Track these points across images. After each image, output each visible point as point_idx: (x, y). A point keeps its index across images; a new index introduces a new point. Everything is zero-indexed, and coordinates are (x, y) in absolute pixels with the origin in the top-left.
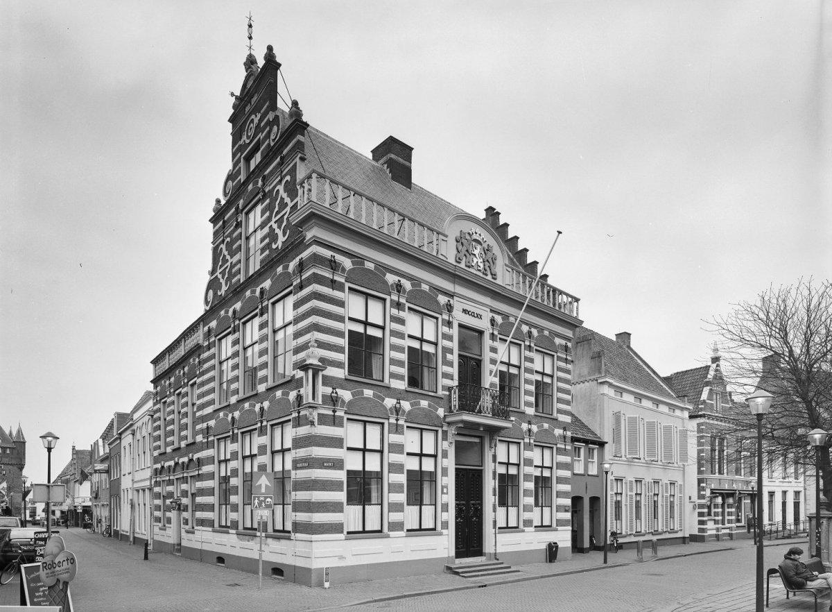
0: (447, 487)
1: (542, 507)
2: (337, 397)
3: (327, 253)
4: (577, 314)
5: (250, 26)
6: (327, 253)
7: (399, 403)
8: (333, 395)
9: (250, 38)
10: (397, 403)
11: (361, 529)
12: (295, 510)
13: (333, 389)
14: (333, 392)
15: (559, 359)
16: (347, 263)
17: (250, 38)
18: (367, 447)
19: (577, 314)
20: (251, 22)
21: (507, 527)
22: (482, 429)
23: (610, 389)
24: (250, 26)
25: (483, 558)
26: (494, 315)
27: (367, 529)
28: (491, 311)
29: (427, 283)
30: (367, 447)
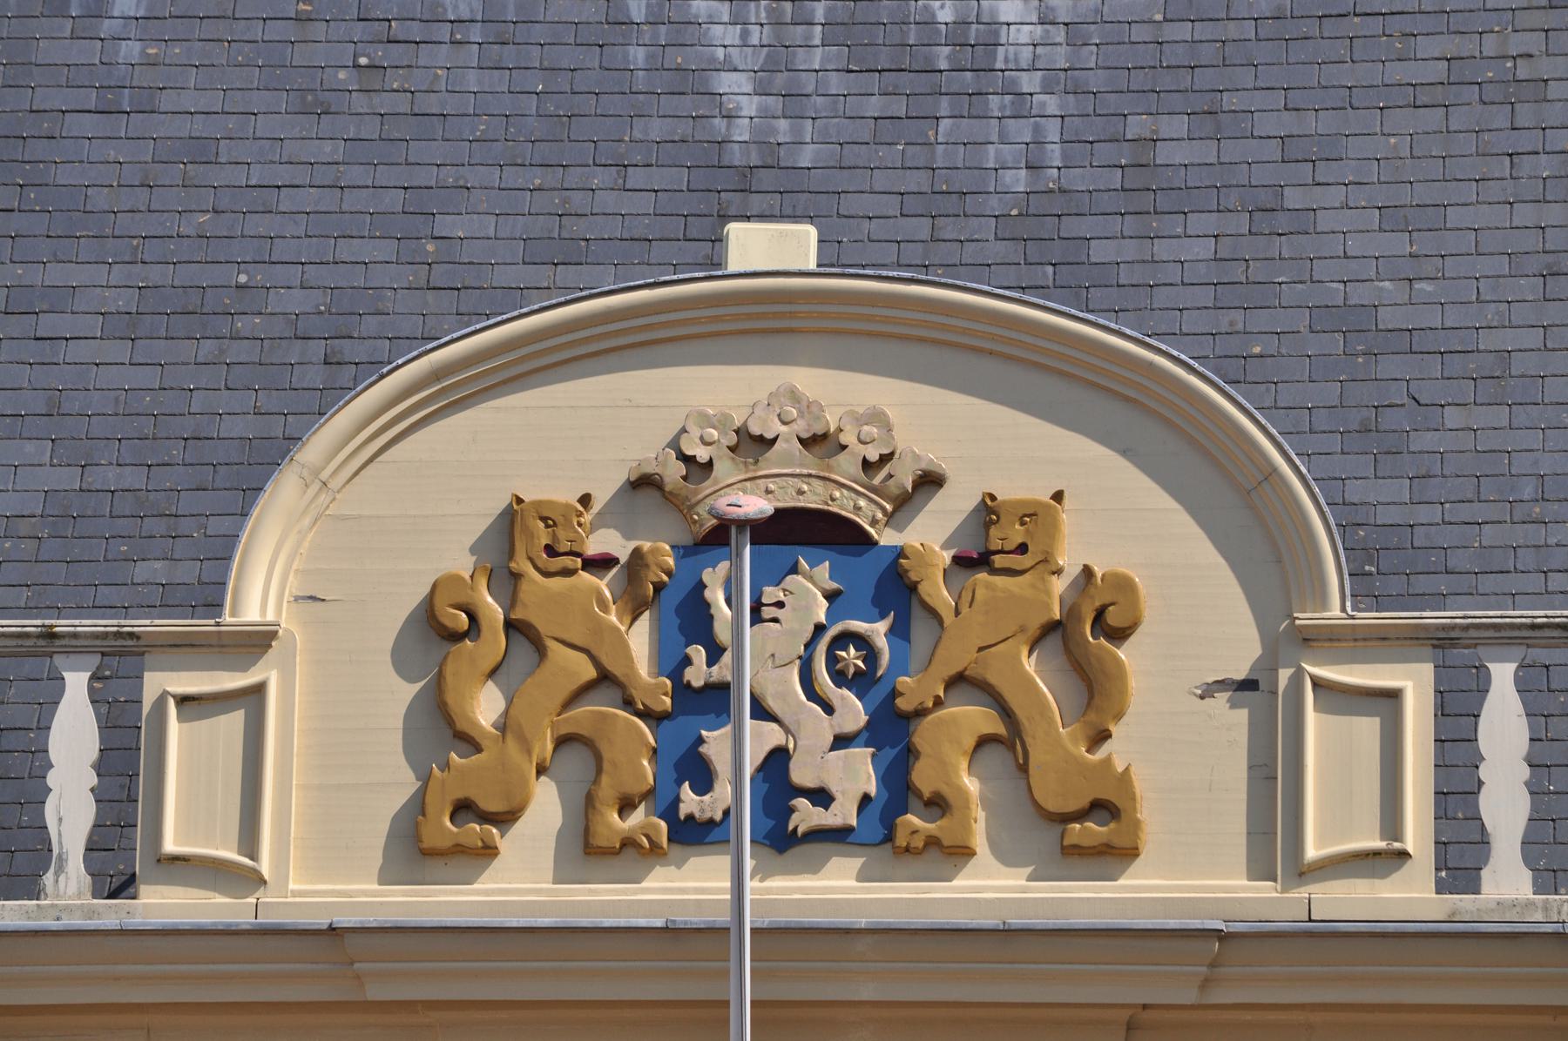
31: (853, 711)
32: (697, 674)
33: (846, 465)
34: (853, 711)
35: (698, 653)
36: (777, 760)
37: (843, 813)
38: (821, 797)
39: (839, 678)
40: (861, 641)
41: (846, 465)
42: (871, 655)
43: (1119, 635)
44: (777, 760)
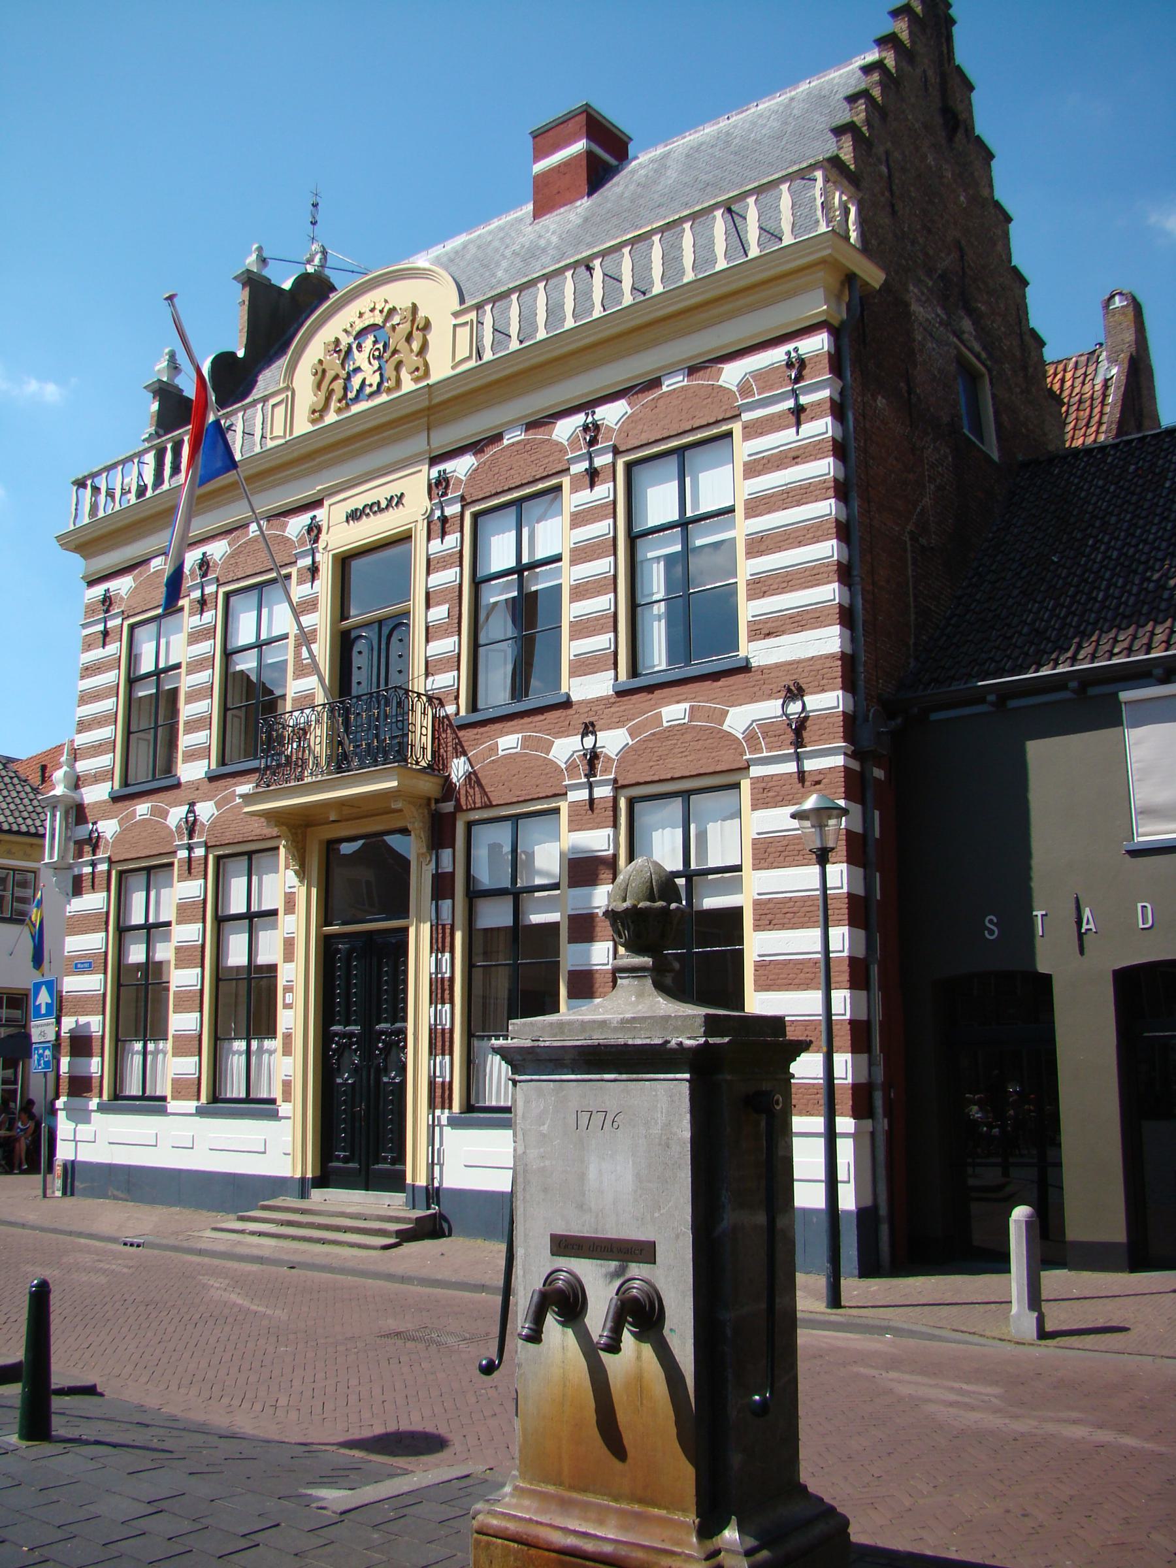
11: (243, 1095)
21: (143, 1098)
26: (441, 467)
31: (376, 364)
33: (368, 314)
34: (376, 364)
36: (364, 381)
38: (371, 385)
39: (374, 358)
40: (378, 349)
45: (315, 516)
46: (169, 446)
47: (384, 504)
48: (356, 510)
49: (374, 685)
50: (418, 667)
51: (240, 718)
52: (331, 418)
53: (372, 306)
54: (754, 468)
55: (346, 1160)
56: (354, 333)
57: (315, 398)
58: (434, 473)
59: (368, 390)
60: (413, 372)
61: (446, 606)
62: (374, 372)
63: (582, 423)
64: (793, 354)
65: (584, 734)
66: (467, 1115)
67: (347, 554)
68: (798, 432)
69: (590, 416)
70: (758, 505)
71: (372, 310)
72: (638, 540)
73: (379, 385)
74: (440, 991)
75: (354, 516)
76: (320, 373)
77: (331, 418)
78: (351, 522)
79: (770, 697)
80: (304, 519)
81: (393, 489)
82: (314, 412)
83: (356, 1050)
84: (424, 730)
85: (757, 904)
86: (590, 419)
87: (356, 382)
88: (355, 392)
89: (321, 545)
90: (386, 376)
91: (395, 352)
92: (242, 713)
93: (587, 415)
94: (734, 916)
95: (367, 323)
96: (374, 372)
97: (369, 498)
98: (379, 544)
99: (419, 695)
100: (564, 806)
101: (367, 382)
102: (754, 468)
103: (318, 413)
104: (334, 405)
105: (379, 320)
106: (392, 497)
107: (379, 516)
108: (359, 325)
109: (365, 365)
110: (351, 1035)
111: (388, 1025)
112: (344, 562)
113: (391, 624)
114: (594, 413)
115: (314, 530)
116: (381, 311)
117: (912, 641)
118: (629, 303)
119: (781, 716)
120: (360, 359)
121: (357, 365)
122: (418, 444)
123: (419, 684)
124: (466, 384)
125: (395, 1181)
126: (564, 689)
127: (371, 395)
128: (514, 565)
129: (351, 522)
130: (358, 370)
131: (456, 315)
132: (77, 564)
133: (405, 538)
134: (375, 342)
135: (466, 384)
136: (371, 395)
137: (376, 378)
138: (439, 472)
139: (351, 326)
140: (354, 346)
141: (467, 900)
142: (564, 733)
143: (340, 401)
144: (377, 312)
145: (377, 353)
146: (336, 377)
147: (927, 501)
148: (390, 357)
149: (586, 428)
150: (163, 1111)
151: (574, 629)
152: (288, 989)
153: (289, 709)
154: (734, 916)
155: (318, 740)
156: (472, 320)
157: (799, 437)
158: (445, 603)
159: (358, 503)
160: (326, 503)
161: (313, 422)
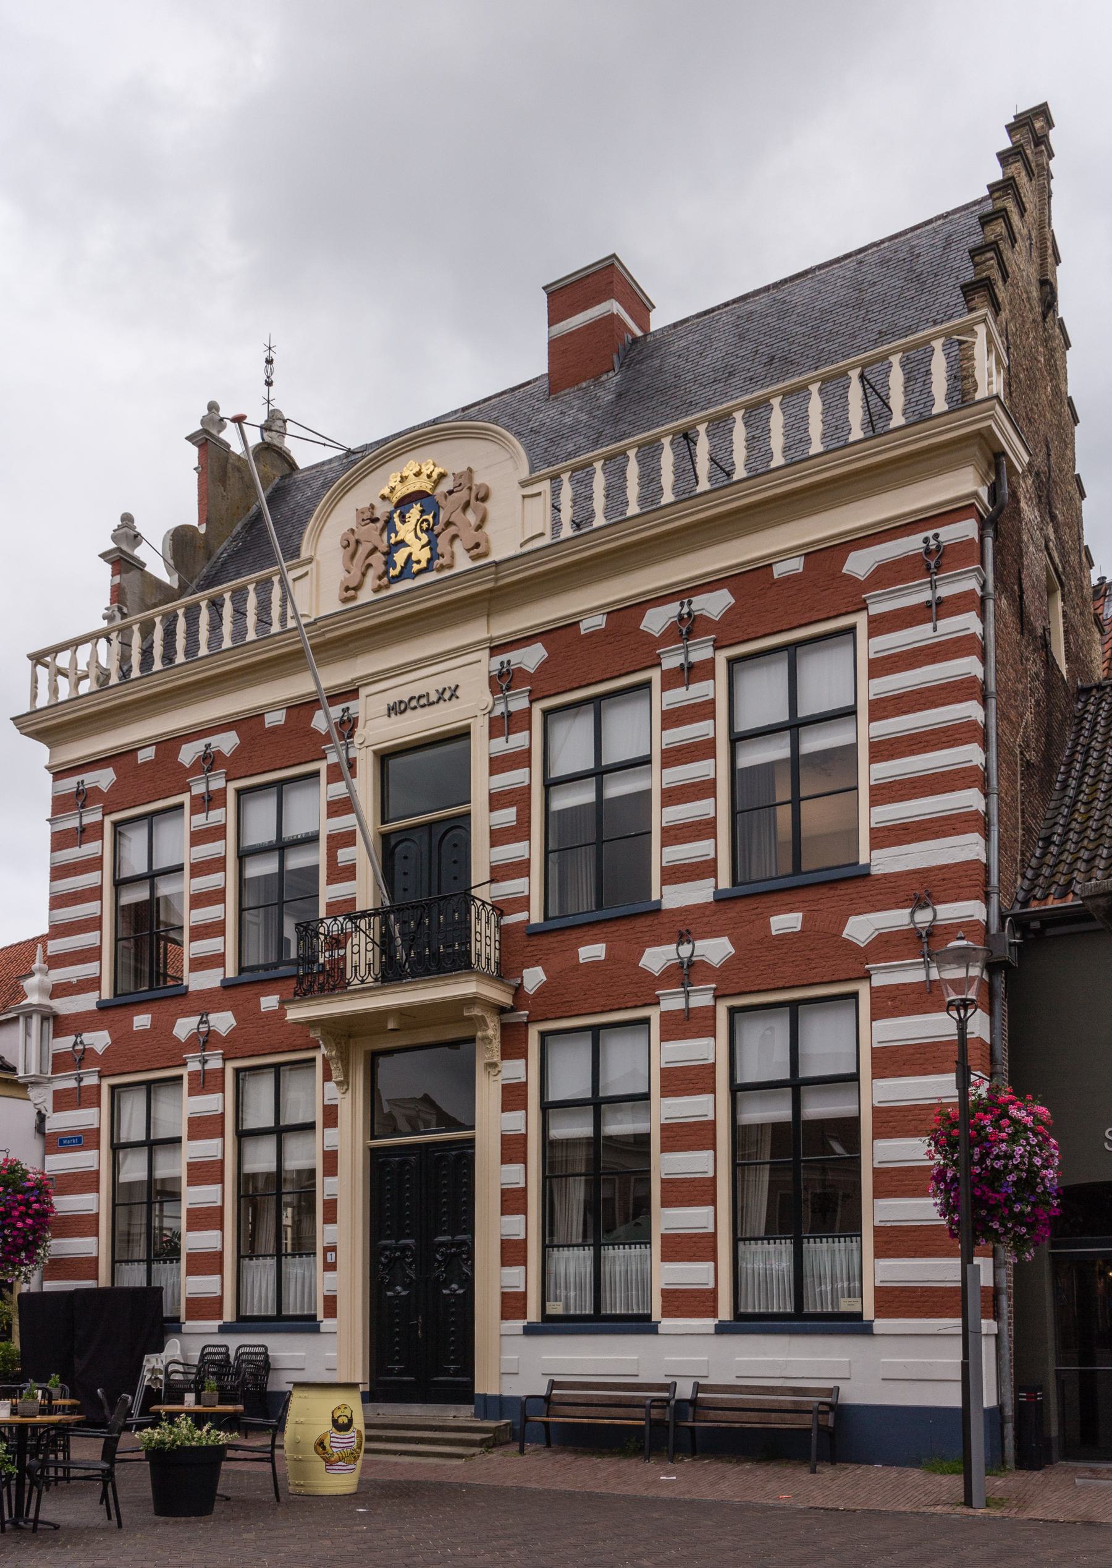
0: (333, 1249)
1: (279, 1255)
2: (85, 1050)
3: (912, 544)
4: (35, 680)
5: (269, 361)
6: (912, 544)
7: (206, 1022)
8: (77, 1048)
9: (269, 384)
10: (201, 1022)
11: (589, 1311)
12: (880, 1252)
13: (77, 1037)
14: (75, 1044)
15: (880, 625)
16: (104, 779)
17: (269, 384)
18: (786, 1075)
19: (35, 680)
20: (272, 354)
21: (279, 1317)
22: (391, 1025)
23: (357, 788)
24: (269, 361)
25: (461, 1414)
26: (504, 657)
27: (809, 1308)
28: (495, 650)
29: (273, 707)
30: (786, 1075)
31: (425, 538)
32: (392, 541)
34: (425, 538)
35: (393, 535)
36: (410, 555)
37: (424, 564)
38: (418, 562)
39: (422, 531)
40: (426, 520)
41: (424, 476)
42: (429, 525)
43: (484, 499)
44: (410, 555)
45: (348, 708)
46: (180, 612)
47: (434, 697)
48: (401, 702)
49: (435, 889)
50: (479, 872)
51: (258, 925)
52: (366, 596)
53: (417, 469)
54: (880, 667)
55: (401, 1373)
56: (395, 500)
57: (348, 575)
58: (496, 663)
59: (416, 567)
60: (472, 549)
61: (514, 810)
62: (423, 547)
63: (676, 613)
64: (932, 542)
65: (680, 943)
66: (737, 1323)
67: (387, 752)
68: (935, 629)
69: (686, 606)
70: (881, 709)
71: (418, 474)
72: (552, 789)
73: (429, 561)
74: (513, 1201)
75: (396, 709)
76: (351, 545)
77: (366, 596)
78: (393, 715)
79: (897, 905)
80: (336, 712)
81: (447, 681)
82: (347, 589)
83: (410, 1264)
84: (488, 943)
85: (664, 1128)
86: (686, 610)
87: (400, 557)
88: (398, 568)
89: (357, 739)
90: (439, 550)
91: (449, 524)
92: (131, 944)
93: (682, 605)
94: (642, 1141)
95: (412, 489)
96: (423, 547)
97: (416, 689)
98: (458, 733)
99: (484, 903)
100: (864, 991)
101: (414, 558)
102: (880, 667)
103: (351, 590)
104: (370, 581)
105: (425, 485)
106: (445, 689)
107: (427, 709)
108: (402, 491)
109: (410, 538)
110: (406, 1247)
111: (449, 1238)
112: (384, 758)
113: (443, 828)
114: (690, 603)
115: (348, 727)
116: (429, 476)
117: (1019, 858)
118: (45, 704)
119: (909, 924)
120: (405, 531)
121: (399, 538)
122: (476, 631)
123: (483, 893)
124: (98, 704)
125: (463, 1393)
126: (655, 896)
127: (421, 572)
128: (593, 766)
129: (393, 715)
130: (402, 543)
131: (524, 484)
132: (41, 752)
133: (463, 735)
134: (422, 512)
135: (98, 704)
136: (421, 572)
137: (426, 554)
138: (502, 663)
139: (391, 492)
140: (396, 515)
141: (111, 1153)
142: (658, 942)
143: (380, 578)
144: (424, 476)
145: (425, 525)
146: (375, 550)
147: (1029, 716)
148: (443, 530)
149: (681, 617)
150: (867, 1330)
151: (875, 793)
152: (331, 1207)
153: (322, 913)
154: (642, 1141)
155: (356, 949)
156: (545, 491)
157: (936, 634)
158: (511, 806)
159: (404, 694)
160: (363, 692)
161: (345, 600)
